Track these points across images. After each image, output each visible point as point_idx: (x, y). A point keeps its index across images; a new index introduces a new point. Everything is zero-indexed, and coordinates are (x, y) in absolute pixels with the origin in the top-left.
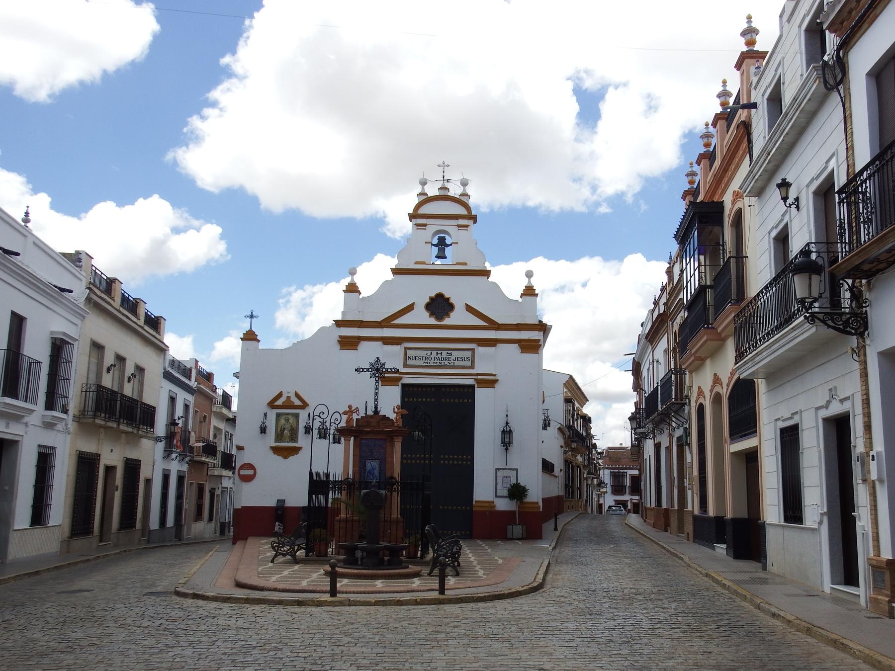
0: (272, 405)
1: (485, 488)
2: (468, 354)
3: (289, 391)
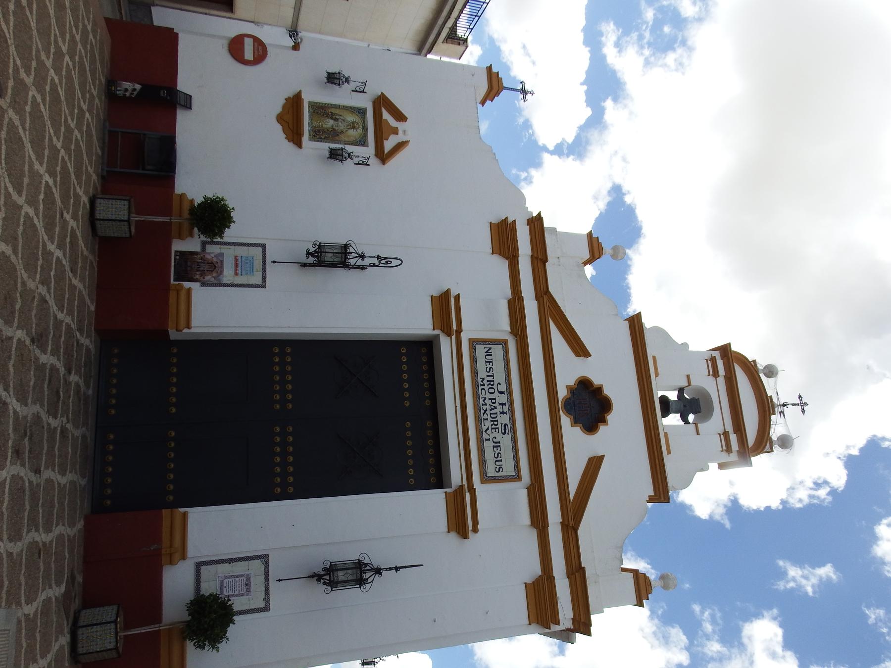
0: (382, 102)
1: (217, 532)
2: (509, 469)
3: (407, 131)
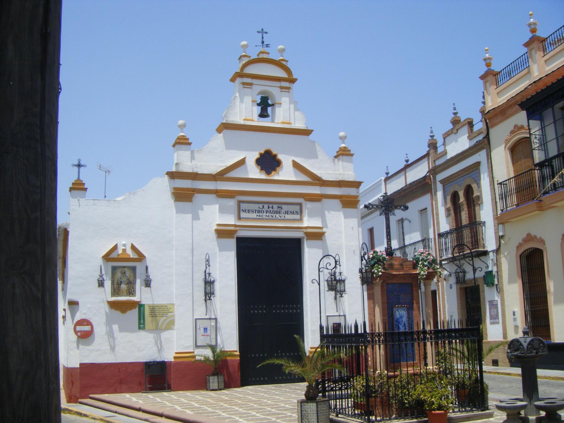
2: (297, 208)
